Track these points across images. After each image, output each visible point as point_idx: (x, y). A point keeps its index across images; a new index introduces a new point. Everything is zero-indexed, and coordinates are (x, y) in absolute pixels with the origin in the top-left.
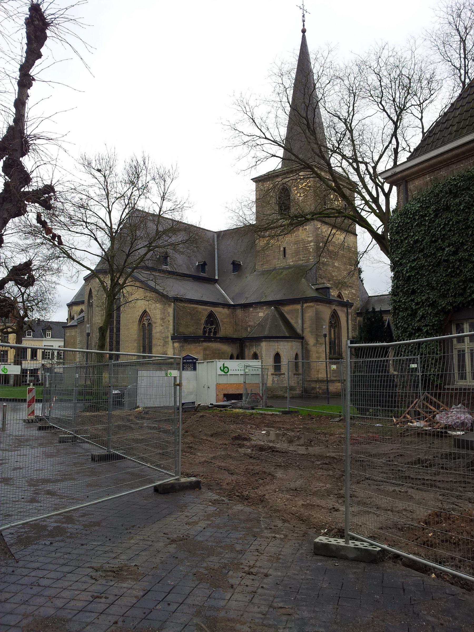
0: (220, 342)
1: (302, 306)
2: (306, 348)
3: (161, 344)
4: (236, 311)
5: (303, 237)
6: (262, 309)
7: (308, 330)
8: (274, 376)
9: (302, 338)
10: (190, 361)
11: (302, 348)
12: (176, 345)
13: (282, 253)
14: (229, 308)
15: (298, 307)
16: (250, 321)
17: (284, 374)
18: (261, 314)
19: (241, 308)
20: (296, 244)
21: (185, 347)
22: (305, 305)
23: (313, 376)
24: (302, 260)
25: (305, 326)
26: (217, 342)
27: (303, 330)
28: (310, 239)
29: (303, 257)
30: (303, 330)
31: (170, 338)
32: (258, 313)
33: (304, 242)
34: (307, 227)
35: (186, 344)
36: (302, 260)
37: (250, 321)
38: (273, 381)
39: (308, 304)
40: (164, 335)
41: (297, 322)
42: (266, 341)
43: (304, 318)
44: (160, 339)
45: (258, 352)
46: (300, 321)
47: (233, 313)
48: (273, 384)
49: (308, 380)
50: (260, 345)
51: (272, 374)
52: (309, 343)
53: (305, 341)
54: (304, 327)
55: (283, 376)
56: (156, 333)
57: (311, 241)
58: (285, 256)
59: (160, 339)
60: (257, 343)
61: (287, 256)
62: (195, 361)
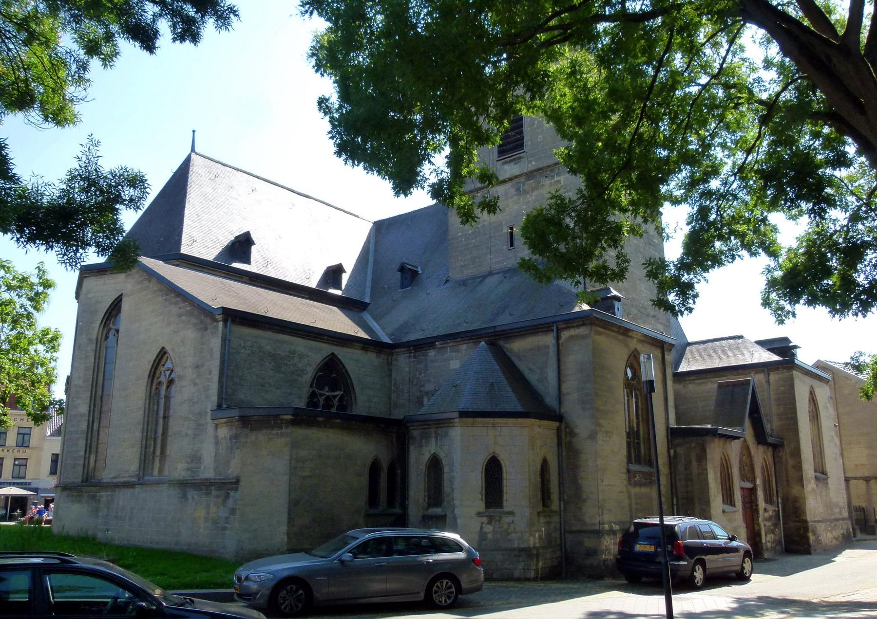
1: (558, 338)
2: (570, 443)
3: (190, 432)
6: (458, 351)
11: (559, 444)
13: (507, 238)
14: (379, 352)
15: (549, 339)
25: (565, 387)
39: (572, 332)
43: (563, 368)
45: (442, 455)
46: (552, 375)
50: (446, 435)
51: (479, 514)
52: (577, 430)
53: (567, 427)
58: (512, 245)
60: (440, 431)
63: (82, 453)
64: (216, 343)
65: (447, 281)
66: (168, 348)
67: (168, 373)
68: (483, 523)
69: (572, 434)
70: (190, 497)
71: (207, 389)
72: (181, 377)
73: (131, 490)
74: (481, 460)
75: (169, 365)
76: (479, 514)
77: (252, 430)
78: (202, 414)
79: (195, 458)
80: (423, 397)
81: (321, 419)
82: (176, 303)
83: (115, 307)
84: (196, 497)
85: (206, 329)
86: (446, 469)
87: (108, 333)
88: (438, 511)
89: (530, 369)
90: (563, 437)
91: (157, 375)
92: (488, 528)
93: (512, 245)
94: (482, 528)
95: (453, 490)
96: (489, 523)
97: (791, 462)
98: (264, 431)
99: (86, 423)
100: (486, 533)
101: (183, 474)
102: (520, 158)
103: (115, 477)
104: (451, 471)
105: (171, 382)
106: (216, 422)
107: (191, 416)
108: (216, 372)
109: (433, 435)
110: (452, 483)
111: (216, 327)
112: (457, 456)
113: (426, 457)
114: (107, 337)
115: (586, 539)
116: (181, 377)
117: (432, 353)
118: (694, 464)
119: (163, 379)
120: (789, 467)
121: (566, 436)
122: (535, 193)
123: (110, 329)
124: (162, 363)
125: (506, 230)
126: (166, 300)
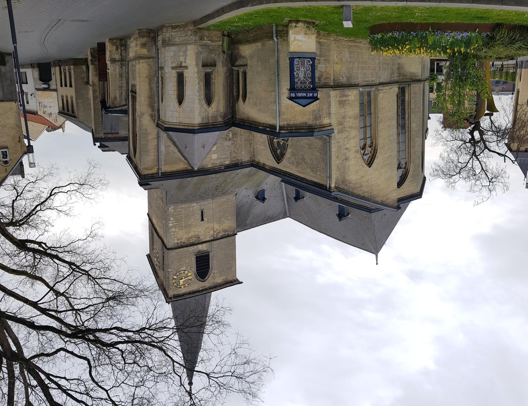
0: (259, 124)
1: (158, 169)
2: (153, 111)
3: (348, 119)
4: (251, 158)
5: (181, 232)
6: (213, 164)
7: (150, 137)
8: (184, 65)
9: (158, 125)
10: (300, 95)
11: (158, 110)
12: (326, 121)
14: (258, 163)
16: (228, 147)
17: (173, 68)
18: (214, 156)
19: (241, 163)
20: (189, 225)
21: (311, 117)
22: (154, 171)
23: (145, 65)
24: (182, 208)
25: (155, 142)
26: (263, 125)
27: (158, 137)
28: (173, 230)
29: (180, 211)
30: (158, 137)
31: (336, 131)
32: (218, 159)
33: (180, 227)
34: (176, 241)
35: (310, 122)
36: (182, 208)
37: (228, 147)
38: (185, 55)
39: (150, 172)
40: (345, 134)
41: (167, 147)
42: (344, 83)
43: (156, 153)
44: (349, 127)
45: (205, 106)
46: (163, 148)
47: (254, 155)
48: (185, 51)
49: (151, 60)
50: (203, 119)
51: (186, 67)
52: (149, 118)
53: (154, 120)
54: (156, 140)
55: (174, 65)
56: (355, 137)
57: (172, 227)
58: (202, 212)
59: (349, 127)
60: (206, 121)
61: (200, 212)
62: (293, 95)
63: (412, 101)
64: (335, 175)
65: (236, 195)
66: (367, 167)
67: (366, 152)
68: (185, 62)
69: (151, 116)
70: (345, 78)
71: (339, 147)
72: (357, 152)
73: (381, 81)
74: (185, 103)
75: (366, 157)
76: (186, 67)
77: (306, 123)
78: (341, 132)
79: (342, 103)
80: (233, 138)
81: (268, 129)
82: (364, 192)
83: (400, 184)
84: (341, 78)
85: (342, 181)
86: (203, 97)
87: (406, 166)
88: (208, 70)
89: (174, 153)
90: (156, 114)
91: (373, 150)
92: (182, 59)
93: (202, 212)
94: (185, 59)
95: (199, 84)
96: (181, 62)
97: (97, 94)
98: (298, 122)
99: (412, 117)
100: (183, 56)
101: (350, 93)
102: (198, 252)
103: (391, 89)
104: (199, 96)
105: (364, 148)
106: (330, 127)
107: (348, 130)
108: (334, 158)
109: (210, 118)
110: (199, 87)
111: (336, 183)
112: (197, 106)
113: (214, 105)
114: (406, 164)
115: (146, 53)
116: (357, 152)
117: (227, 162)
118: (118, 96)
119: (368, 150)
120: (98, 91)
121: (155, 115)
122: (190, 236)
123: (404, 168)
124: (370, 158)
125: (205, 219)
126: (371, 193)
